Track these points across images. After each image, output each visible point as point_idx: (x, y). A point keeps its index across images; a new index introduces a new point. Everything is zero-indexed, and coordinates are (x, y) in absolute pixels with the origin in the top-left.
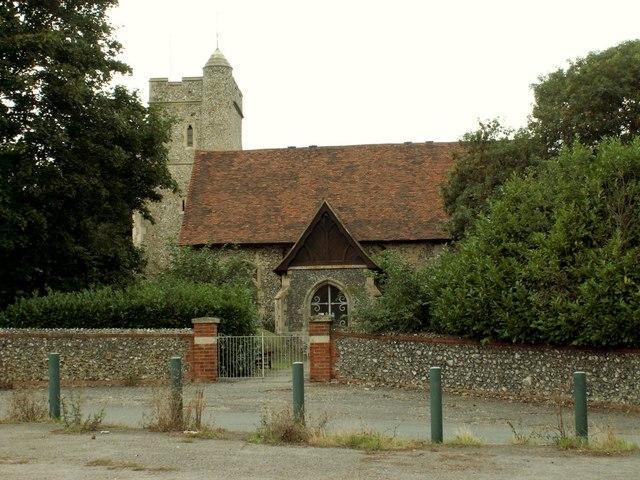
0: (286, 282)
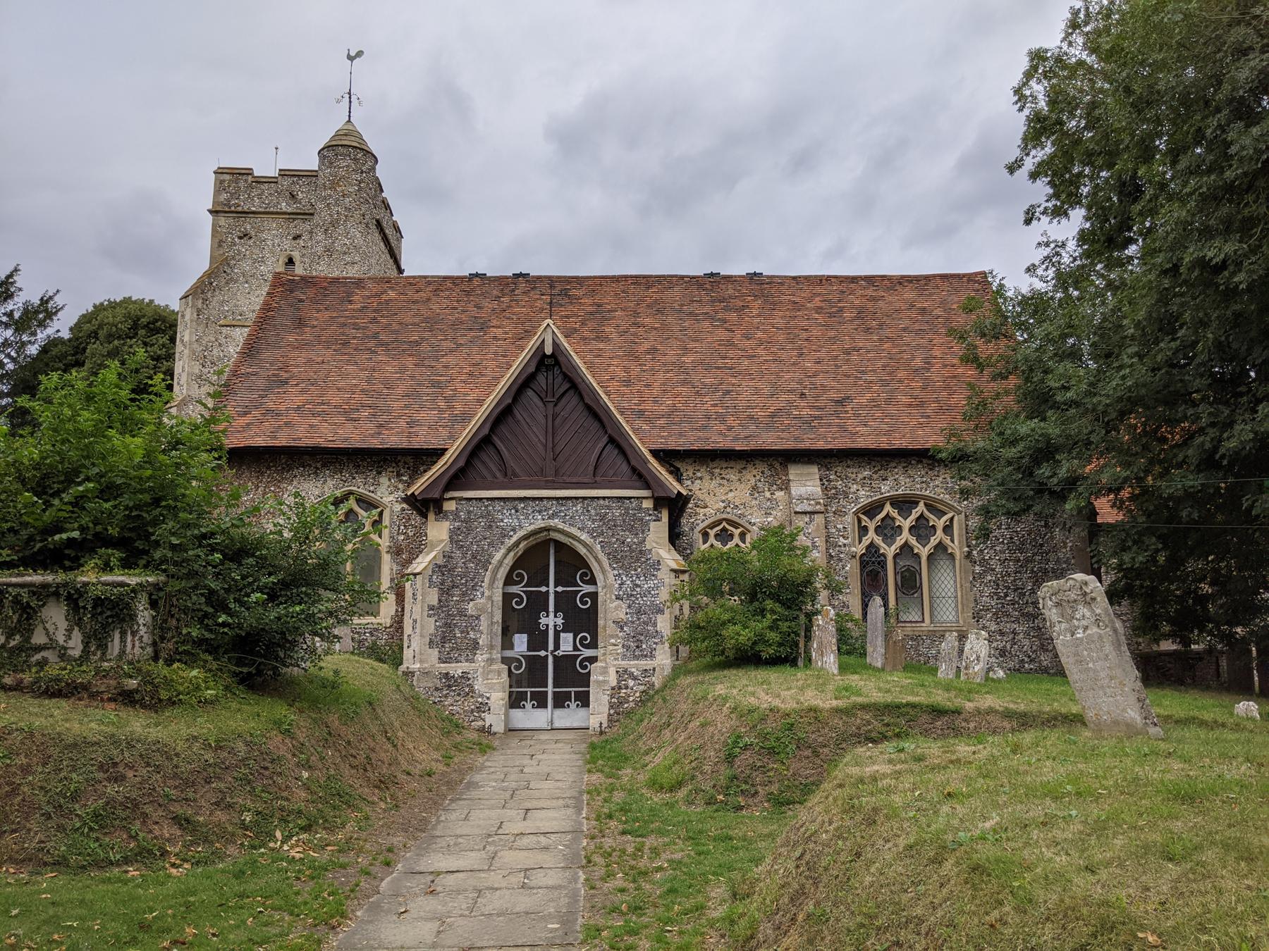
0: (438, 531)
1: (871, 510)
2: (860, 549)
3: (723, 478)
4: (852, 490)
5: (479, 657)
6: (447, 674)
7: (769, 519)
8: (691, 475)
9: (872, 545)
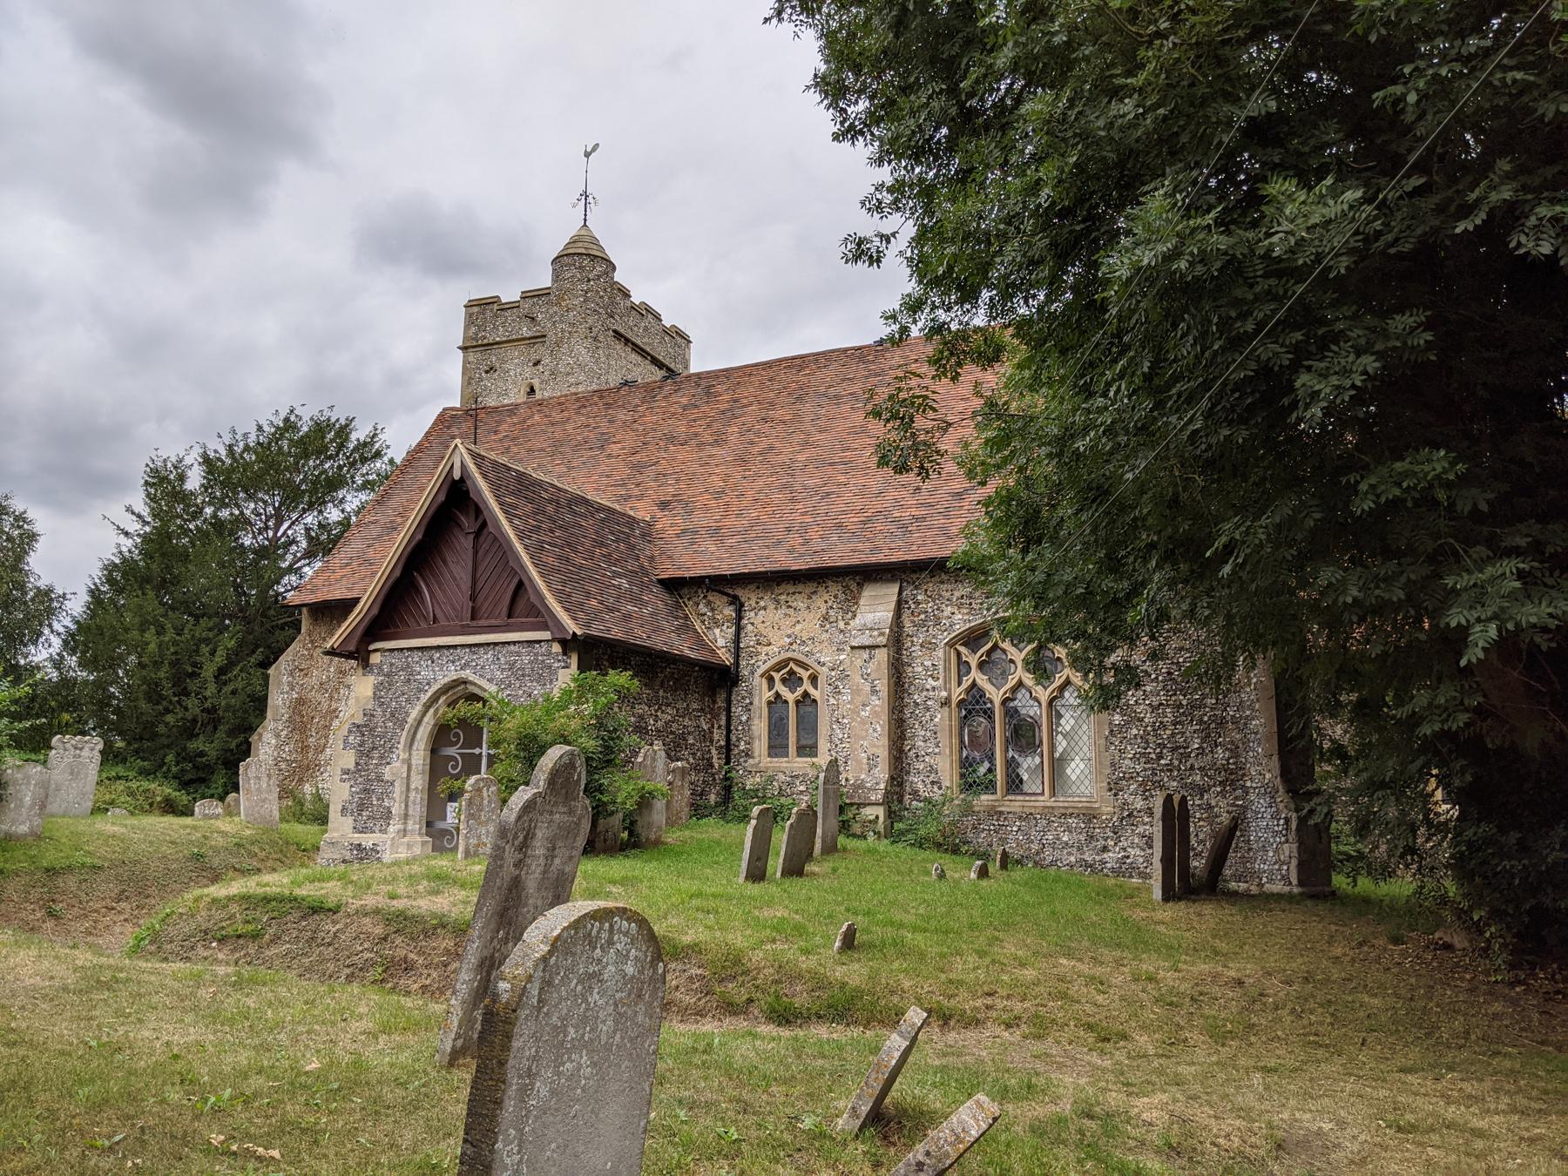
1: (973, 638)
2: (958, 693)
3: (790, 607)
4: (945, 614)
5: (391, 829)
6: (360, 845)
7: (842, 657)
8: (754, 605)
9: (974, 684)
